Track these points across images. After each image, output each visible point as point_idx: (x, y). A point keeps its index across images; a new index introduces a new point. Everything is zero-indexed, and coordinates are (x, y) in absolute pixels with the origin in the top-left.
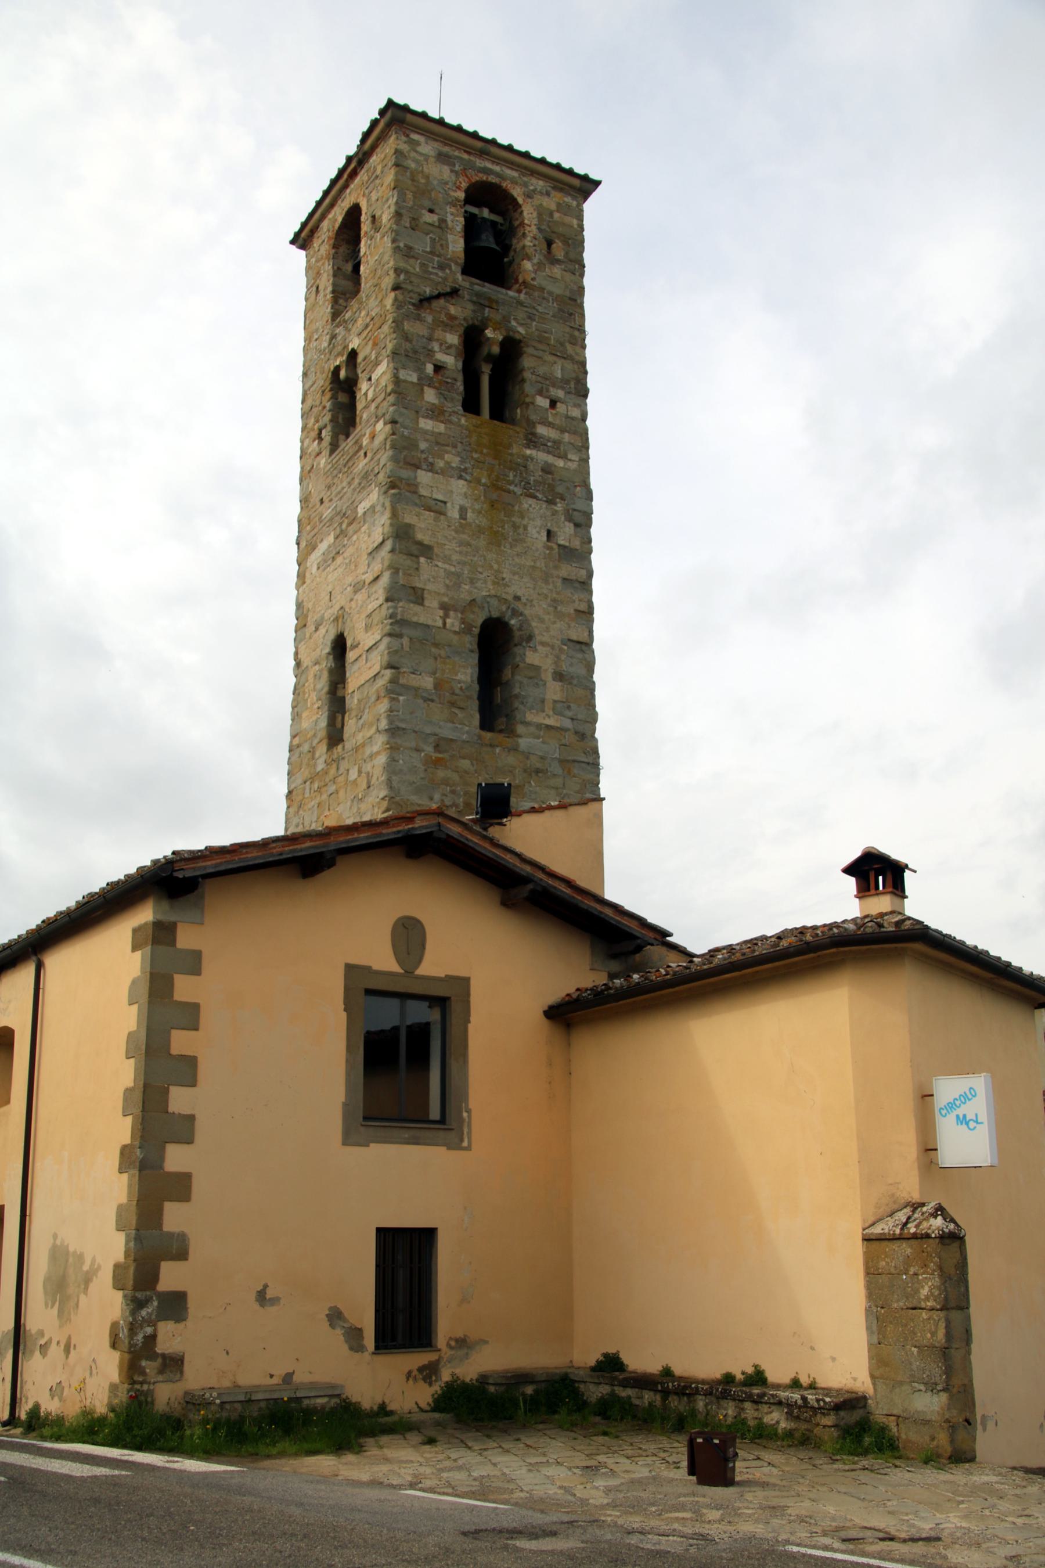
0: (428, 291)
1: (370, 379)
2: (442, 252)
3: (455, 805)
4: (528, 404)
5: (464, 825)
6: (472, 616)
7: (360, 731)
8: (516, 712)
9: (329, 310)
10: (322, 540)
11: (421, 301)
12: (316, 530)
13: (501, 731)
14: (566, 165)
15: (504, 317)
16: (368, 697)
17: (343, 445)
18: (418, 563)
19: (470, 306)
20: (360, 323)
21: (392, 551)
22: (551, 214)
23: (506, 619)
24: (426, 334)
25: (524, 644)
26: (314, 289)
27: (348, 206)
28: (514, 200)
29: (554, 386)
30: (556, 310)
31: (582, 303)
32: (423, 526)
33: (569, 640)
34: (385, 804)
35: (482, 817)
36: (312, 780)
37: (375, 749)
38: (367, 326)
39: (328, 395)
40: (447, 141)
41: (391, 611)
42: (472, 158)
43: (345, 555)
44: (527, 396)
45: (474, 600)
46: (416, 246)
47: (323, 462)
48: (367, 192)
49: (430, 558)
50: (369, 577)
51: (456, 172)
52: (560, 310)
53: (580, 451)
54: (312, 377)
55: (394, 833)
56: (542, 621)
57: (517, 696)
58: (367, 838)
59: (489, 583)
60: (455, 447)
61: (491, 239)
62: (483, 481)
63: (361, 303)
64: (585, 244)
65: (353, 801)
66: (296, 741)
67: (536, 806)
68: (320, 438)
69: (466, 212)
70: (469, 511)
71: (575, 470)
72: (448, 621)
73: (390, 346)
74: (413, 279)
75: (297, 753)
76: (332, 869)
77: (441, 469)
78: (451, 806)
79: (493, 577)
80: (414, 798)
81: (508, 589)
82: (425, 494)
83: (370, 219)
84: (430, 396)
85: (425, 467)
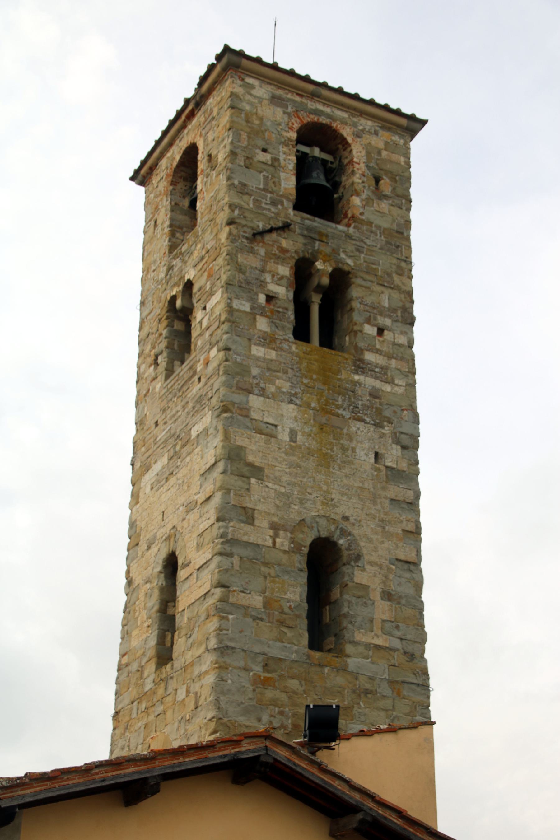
0: (261, 225)
1: (205, 308)
2: (275, 189)
3: (283, 726)
4: (356, 333)
5: (291, 748)
6: (301, 536)
7: (189, 650)
8: (345, 632)
9: (166, 243)
10: (156, 462)
11: (254, 235)
12: (151, 451)
13: (329, 651)
14: (394, 106)
15: (333, 250)
16: (198, 616)
17: (178, 370)
18: (249, 484)
19: (301, 240)
20: (196, 255)
21: (224, 472)
22: (379, 152)
23: (335, 539)
24: (259, 267)
25: (353, 563)
26: (153, 223)
27: (186, 146)
28: (344, 140)
29: (381, 315)
30: (384, 243)
31: (409, 236)
32: (254, 448)
33: (397, 560)
34: (212, 725)
35: (310, 740)
36: (139, 699)
37: (204, 668)
38: (202, 258)
39: (165, 323)
40: (280, 84)
41: (222, 530)
42: (304, 100)
43: (178, 476)
44: (356, 324)
45: (303, 520)
46: (250, 184)
47: (158, 386)
48: (204, 132)
49: (260, 479)
50: (201, 498)
51: (289, 114)
52: (388, 243)
53: (407, 376)
54: (149, 306)
55: (221, 757)
56: (370, 541)
57: (345, 616)
58: (193, 762)
59: (319, 503)
60: (286, 372)
61: (322, 177)
62: (313, 405)
63: (197, 236)
64: (412, 180)
65: (180, 722)
66: (125, 660)
67: (365, 729)
68: (156, 363)
69: (298, 151)
70: (299, 433)
71: (402, 395)
72: (278, 540)
73: (224, 278)
74: (247, 214)
75: (126, 671)
76: (155, 796)
77: (272, 393)
78: (280, 728)
79: (322, 498)
80: (242, 720)
81: (337, 510)
82: (257, 418)
83: (206, 158)
84: (262, 324)
85: (256, 392)
